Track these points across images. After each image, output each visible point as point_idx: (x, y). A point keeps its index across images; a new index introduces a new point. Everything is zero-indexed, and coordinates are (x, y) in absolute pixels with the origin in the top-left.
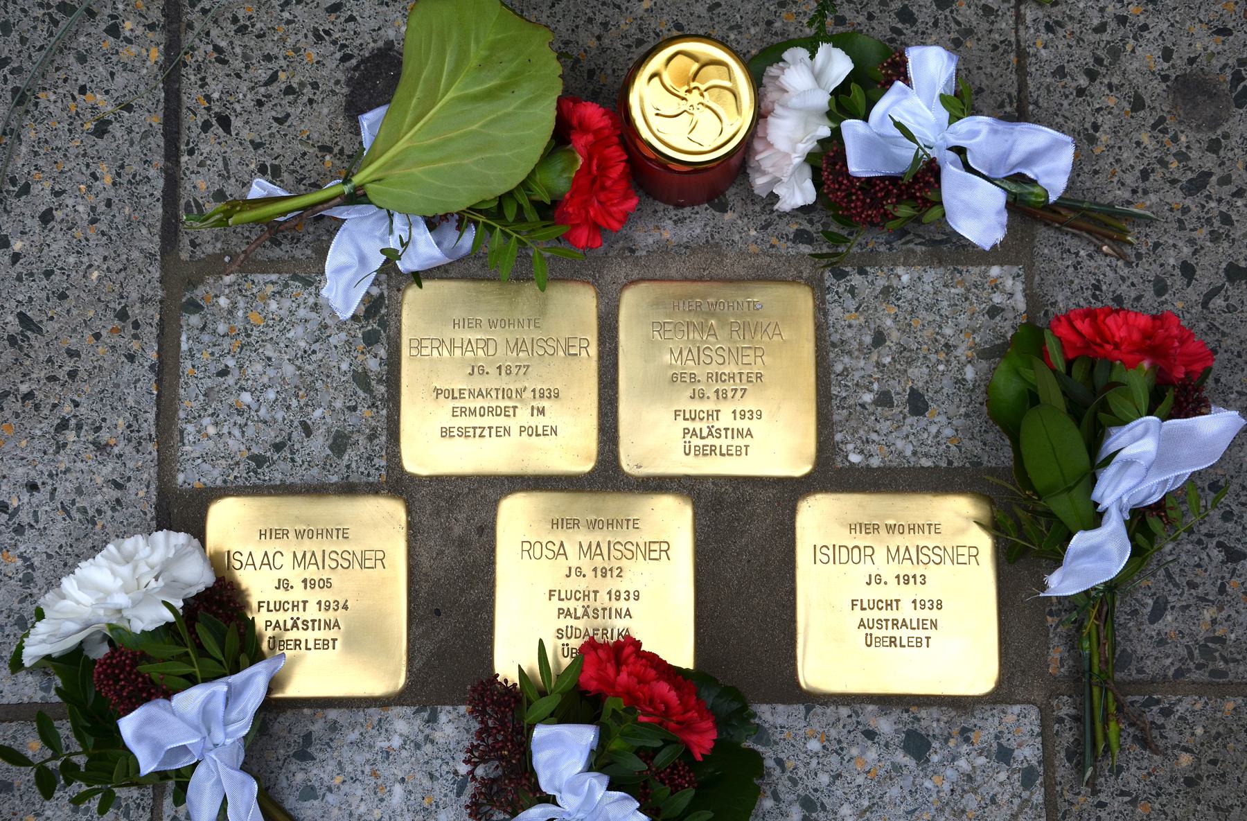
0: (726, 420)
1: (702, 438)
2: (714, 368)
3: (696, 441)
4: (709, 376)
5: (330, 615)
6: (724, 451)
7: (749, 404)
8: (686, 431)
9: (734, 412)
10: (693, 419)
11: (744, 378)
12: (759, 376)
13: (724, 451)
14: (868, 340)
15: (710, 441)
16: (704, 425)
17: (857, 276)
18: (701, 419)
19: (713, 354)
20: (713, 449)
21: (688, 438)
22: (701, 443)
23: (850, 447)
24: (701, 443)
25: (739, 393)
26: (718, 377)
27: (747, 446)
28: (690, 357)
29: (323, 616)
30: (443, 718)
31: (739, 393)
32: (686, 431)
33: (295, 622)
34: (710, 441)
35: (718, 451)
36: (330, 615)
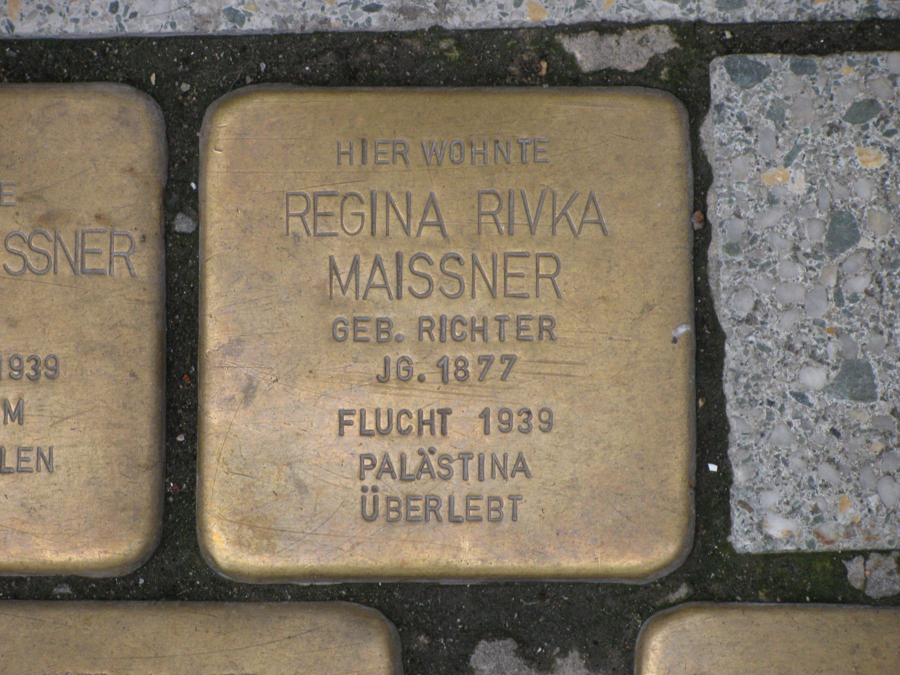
0: (463, 431)
1: (405, 478)
2: (434, 308)
3: (391, 486)
4: (423, 325)
5: (511, 445)
6: (459, 510)
7: (527, 393)
8: (366, 462)
9: (485, 415)
10: (383, 433)
11: (510, 329)
12: (547, 328)
13: (459, 510)
14: (815, 235)
15: (423, 486)
16: (409, 447)
17: (792, 78)
18: (403, 433)
19: (434, 272)
20: (432, 505)
21: (369, 479)
22: (397, 488)
23: (771, 499)
24: (397, 488)
25: (497, 368)
26: (445, 328)
27: (514, 499)
28: (378, 279)
29: (493, 444)
30: (876, 533)
31: (497, 368)
32: (366, 462)
33: (425, 461)
34: (423, 486)
35: (443, 512)
36: (511, 445)
